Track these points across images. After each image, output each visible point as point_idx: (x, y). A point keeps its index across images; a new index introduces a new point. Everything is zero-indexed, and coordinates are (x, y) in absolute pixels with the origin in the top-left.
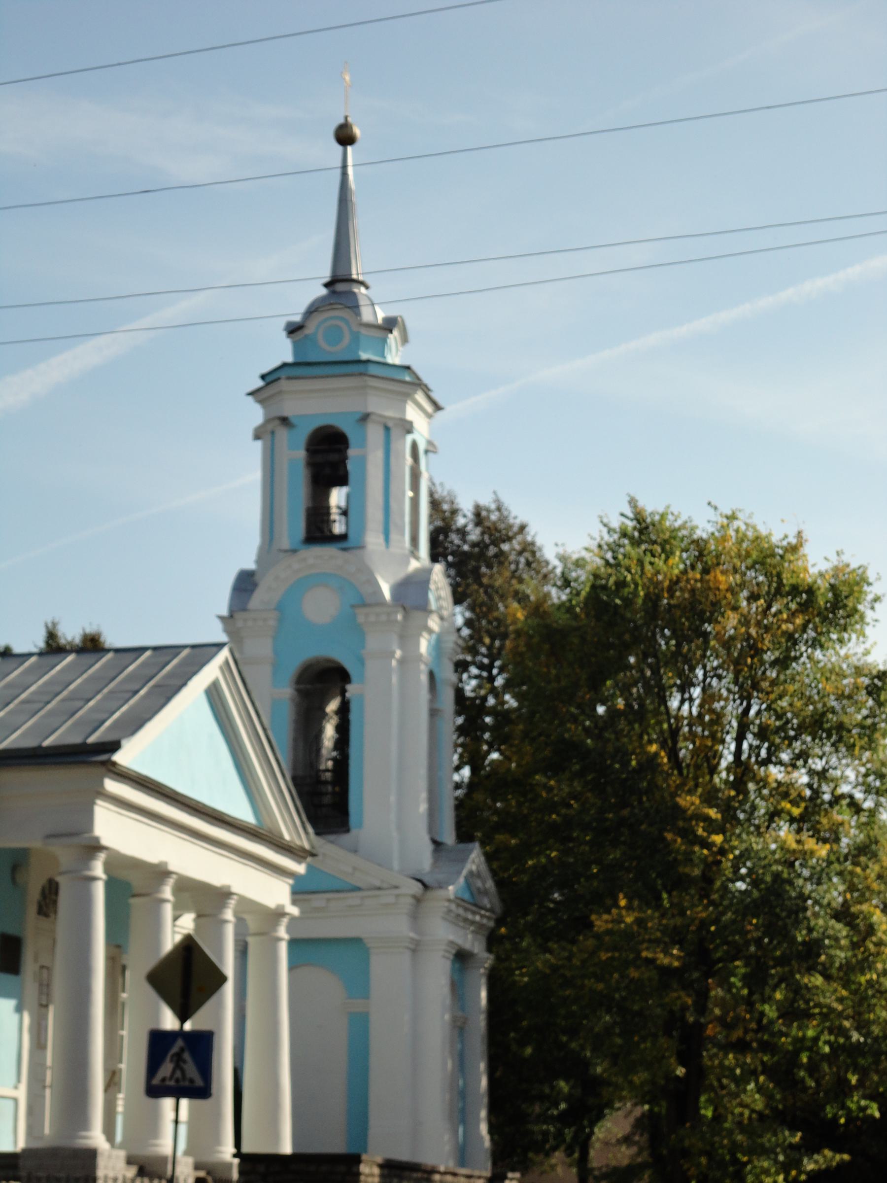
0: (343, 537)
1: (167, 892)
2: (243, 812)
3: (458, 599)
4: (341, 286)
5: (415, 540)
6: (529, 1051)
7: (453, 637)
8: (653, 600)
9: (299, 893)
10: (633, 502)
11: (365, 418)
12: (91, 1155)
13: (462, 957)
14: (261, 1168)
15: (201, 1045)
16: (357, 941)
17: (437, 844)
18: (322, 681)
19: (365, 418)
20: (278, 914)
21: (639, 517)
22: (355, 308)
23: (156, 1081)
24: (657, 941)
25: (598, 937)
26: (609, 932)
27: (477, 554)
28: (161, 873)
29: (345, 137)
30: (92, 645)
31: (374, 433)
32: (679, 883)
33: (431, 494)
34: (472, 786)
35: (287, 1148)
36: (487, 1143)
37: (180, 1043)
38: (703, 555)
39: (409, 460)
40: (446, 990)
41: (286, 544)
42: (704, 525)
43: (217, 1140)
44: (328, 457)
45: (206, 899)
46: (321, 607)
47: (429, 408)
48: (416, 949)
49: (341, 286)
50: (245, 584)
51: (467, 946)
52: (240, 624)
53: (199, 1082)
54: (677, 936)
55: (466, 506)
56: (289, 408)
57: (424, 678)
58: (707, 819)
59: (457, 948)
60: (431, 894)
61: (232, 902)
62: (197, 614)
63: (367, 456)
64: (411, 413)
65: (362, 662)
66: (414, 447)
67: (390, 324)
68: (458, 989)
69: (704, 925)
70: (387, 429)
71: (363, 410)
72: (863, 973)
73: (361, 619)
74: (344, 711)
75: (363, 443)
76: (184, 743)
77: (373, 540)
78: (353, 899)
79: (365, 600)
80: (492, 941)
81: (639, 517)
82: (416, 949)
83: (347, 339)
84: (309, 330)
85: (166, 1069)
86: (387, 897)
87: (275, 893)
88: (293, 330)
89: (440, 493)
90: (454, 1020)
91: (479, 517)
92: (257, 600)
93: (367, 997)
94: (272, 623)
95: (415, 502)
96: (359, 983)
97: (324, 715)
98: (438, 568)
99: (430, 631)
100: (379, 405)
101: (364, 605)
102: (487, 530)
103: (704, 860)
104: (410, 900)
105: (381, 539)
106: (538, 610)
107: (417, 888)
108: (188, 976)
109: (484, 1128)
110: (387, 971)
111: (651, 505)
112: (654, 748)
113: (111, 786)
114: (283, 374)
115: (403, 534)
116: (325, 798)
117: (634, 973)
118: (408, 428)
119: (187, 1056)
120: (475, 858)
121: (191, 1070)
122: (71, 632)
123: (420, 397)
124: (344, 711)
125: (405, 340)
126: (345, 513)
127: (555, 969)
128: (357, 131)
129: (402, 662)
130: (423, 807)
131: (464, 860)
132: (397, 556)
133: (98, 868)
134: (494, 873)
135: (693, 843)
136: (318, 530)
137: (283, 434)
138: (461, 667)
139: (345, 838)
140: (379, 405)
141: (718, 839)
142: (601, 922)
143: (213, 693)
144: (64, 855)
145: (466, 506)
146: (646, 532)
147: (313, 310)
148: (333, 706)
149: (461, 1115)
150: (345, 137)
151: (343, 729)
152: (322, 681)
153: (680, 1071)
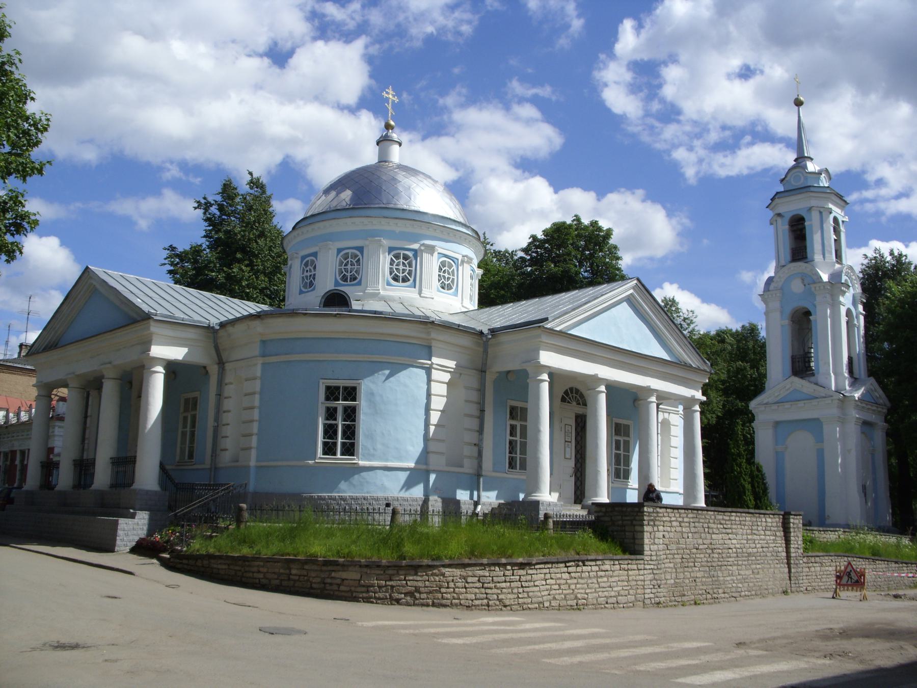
11: (810, 209)
13: (866, 424)
16: (818, 419)
19: (810, 209)
28: (649, 391)
31: (815, 215)
41: (783, 262)
56: (781, 210)
59: (165, 364)
65: (815, 306)
70: (821, 213)
71: (809, 206)
72: (219, 238)
77: (818, 257)
78: (814, 402)
86: (828, 401)
92: (772, 287)
93: (822, 442)
96: (819, 438)
101: (814, 283)
105: (821, 257)
115: (831, 254)
137: (779, 220)
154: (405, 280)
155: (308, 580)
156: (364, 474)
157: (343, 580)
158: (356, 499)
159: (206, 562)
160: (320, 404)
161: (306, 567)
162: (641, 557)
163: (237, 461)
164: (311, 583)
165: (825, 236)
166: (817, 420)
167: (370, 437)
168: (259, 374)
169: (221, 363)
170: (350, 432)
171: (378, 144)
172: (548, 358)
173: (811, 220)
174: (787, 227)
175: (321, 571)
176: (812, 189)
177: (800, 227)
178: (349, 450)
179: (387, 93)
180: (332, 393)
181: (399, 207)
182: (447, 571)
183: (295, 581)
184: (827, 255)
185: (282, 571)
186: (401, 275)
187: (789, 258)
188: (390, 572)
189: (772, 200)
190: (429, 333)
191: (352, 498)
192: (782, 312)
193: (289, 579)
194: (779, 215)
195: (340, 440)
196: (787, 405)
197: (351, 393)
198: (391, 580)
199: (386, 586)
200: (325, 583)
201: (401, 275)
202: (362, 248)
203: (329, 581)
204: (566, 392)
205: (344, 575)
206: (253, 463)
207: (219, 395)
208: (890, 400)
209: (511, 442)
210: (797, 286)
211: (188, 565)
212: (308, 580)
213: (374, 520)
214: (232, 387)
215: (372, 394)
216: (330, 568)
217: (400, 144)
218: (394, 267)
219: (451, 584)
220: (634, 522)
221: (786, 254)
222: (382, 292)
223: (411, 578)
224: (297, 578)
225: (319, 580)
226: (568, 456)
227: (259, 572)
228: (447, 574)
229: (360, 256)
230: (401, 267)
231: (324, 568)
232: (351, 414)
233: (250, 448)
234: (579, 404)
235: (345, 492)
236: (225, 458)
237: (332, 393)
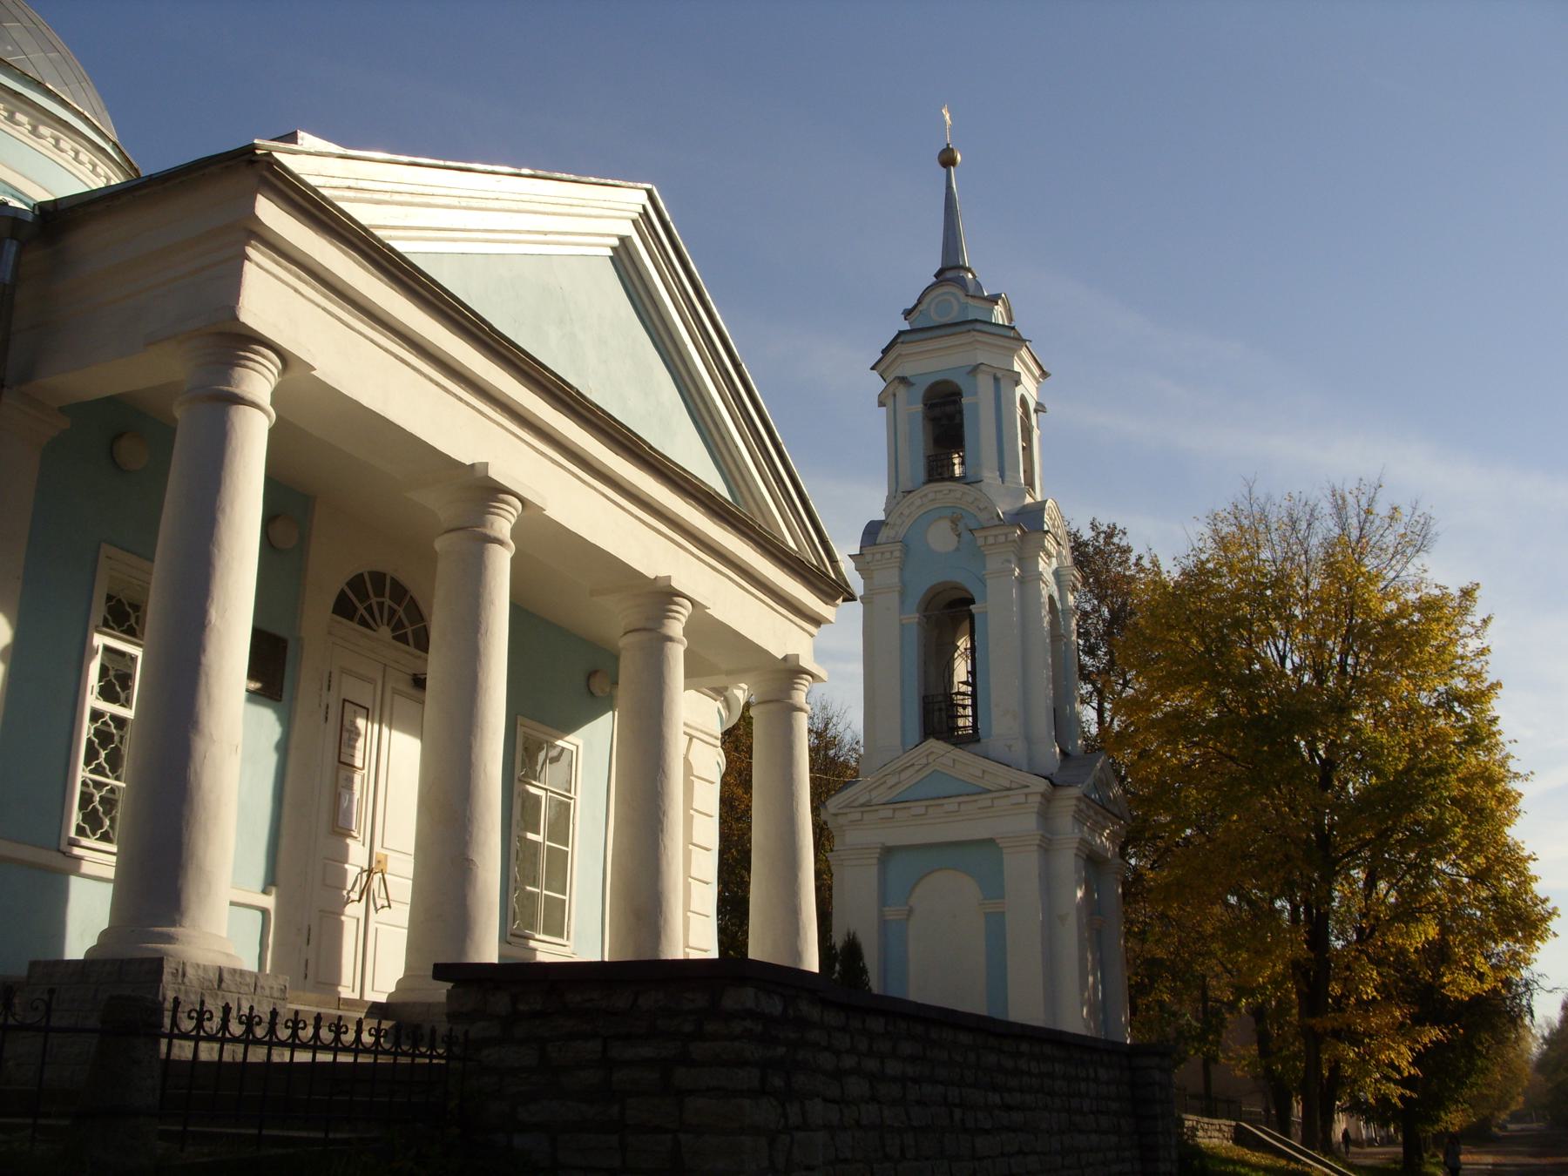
4: (950, 272)
11: (975, 370)
14: (500, 1003)
16: (991, 841)
19: (975, 370)
31: (984, 383)
39: (1019, 411)
41: (906, 484)
47: (1037, 372)
49: (950, 272)
52: (868, 558)
56: (908, 369)
65: (983, 582)
70: (996, 379)
73: (980, 542)
77: (990, 475)
78: (984, 801)
83: (956, 307)
94: (897, 554)
104: (1038, 798)
107: (1042, 785)
110: (1021, 867)
136: (937, 470)
137: (902, 392)
173: (975, 393)
174: (919, 407)
176: (979, 326)
184: (1007, 473)
187: (921, 474)
189: (885, 351)
192: (903, 594)
194: (903, 380)
196: (918, 808)
204: (356, 583)
210: (941, 538)
221: (915, 466)
223: (167, 1021)
226: (989, 803)
234: (402, 639)
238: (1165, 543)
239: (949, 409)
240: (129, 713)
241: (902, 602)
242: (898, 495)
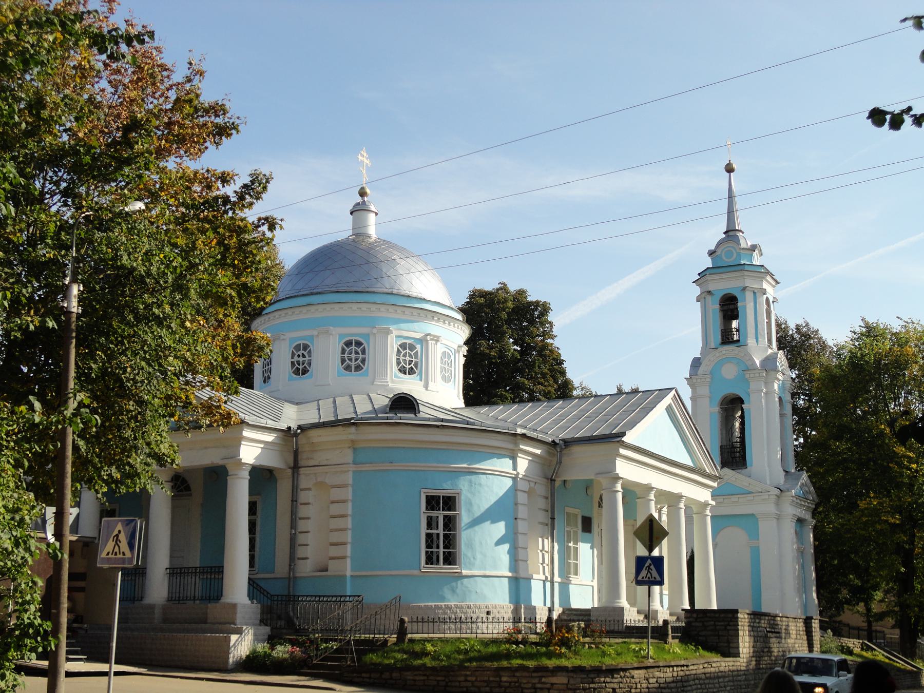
0: (738, 341)
1: (652, 496)
2: (688, 462)
3: (792, 367)
4: (731, 233)
5: (770, 341)
6: (836, 562)
7: (790, 382)
8: (878, 362)
9: (714, 496)
10: (863, 320)
11: (744, 289)
12: (622, 609)
13: (800, 521)
15: (659, 562)
16: (753, 515)
17: (787, 472)
18: (732, 405)
19: (744, 289)
20: (706, 504)
21: (867, 326)
22: (738, 243)
23: (640, 578)
24: (888, 512)
25: (862, 511)
26: (866, 509)
27: (797, 346)
28: (649, 488)
29: (729, 169)
30: (635, 391)
31: (749, 295)
32: (899, 486)
33: (776, 321)
34: (803, 446)
35: (715, 607)
36: (816, 602)
37: (649, 561)
38: (899, 340)
39: (765, 307)
40: (794, 535)
42: (896, 326)
43: (681, 601)
44: (729, 307)
45: (672, 500)
46: (729, 372)
47: (774, 283)
48: (779, 518)
49: (731, 233)
50: (696, 363)
51: (802, 516)
52: (694, 381)
53: (658, 579)
54: (899, 510)
55: (792, 325)
56: (711, 287)
57: (777, 399)
58: (909, 457)
60: (784, 494)
61: (683, 500)
62: (676, 376)
63: (747, 306)
64: (765, 286)
66: (767, 299)
67: (753, 248)
68: (799, 535)
69: (910, 504)
70: (754, 293)
73: (747, 376)
74: (742, 417)
75: (744, 300)
76: (655, 431)
77: (751, 341)
78: (750, 497)
79: (749, 367)
80: (814, 513)
81: (867, 326)
82: (779, 518)
84: (718, 253)
85: (644, 573)
86: (765, 496)
87: (704, 495)
88: (711, 253)
89: (781, 320)
90: (798, 548)
91: (798, 328)
92: (701, 370)
95: (769, 324)
96: (754, 533)
97: (734, 418)
98: (781, 352)
99: (779, 380)
100: (751, 283)
102: (802, 335)
103: (908, 476)
106: (826, 369)
108: (651, 533)
109: (814, 595)
110: (767, 528)
111: (871, 320)
112: (883, 427)
113: (622, 451)
114: (707, 272)
116: (733, 455)
117: (878, 527)
118: (764, 292)
119: (652, 567)
120: (805, 476)
121: (654, 573)
122: (627, 388)
123: (769, 278)
124: (742, 417)
125: (761, 254)
126: (738, 331)
127: (843, 525)
128: (735, 166)
129: (766, 394)
130: (779, 456)
131: (798, 479)
132: (761, 348)
133: (619, 487)
134: (814, 484)
135: (903, 468)
136: (727, 338)
137: (709, 298)
138: (793, 395)
139: (744, 471)
140: (751, 283)
141: (914, 466)
142: (862, 504)
143: (669, 409)
144: (604, 482)
145: (792, 325)
146: (871, 332)
147: (719, 244)
148: (739, 414)
149: (803, 588)
150: (729, 169)
151: (742, 424)
152: (732, 405)
153: (903, 570)
154: (412, 371)
155: (519, 686)
156: (465, 581)
157: (552, 684)
158: (461, 608)
159: (395, 675)
160: (422, 515)
161: (517, 674)
162: (738, 659)
163: (327, 570)
164: (523, 688)
165: (758, 319)
166: (752, 517)
167: (470, 546)
168: (350, 482)
169: (296, 467)
170: (450, 541)
171: (351, 213)
172: (626, 470)
174: (717, 306)
175: (532, 677)
176: (746, 268)
177: (732, 307)
178: (450, 559)
179: (362, 156)
180: (432, 503)
181: (403, 292)
182: (636, 673)
183: (506, 688)
185: (491, 679)
186: (408, 367)
188: (592, 676)
190: (517, 445)
191: (457, 607)
193: (500, 686)
194: (709, 292)
195: (441, 550)
197: (450, 502)
198: (593, 683)
199: (590, 688)
200: (535, 688)
201: (408, 367)
202: (368, 335)
203: (539, 686)
205: (554, 680)
206: (349, 573)
207: (294, 500)
208: (818, 496)
209: (429, 536)
211: (370, 678)
212: (519, 686)
213: (478, 628)
214: (311, 493)
215: (471, 504)
216: (540, 674)
217: (376, 214)
218: (401, 358)
219: (639, 686)
220: (728, 628)
222: (390, 385)
224: (507, 684)
225: (530, 685)
227: (466, 681)
228: (636, 676)
229: (365, 345)
230: (353, 356)
231: (535, 675)
232: (450, 523)
233: (344, 558)
235: (449, 601)
236: (305, 569)
237: (432, 503)
238: (837, 333)
239: (732, 307)
240: (486, 554)
241: (711, 401)
242: (706, 347)
